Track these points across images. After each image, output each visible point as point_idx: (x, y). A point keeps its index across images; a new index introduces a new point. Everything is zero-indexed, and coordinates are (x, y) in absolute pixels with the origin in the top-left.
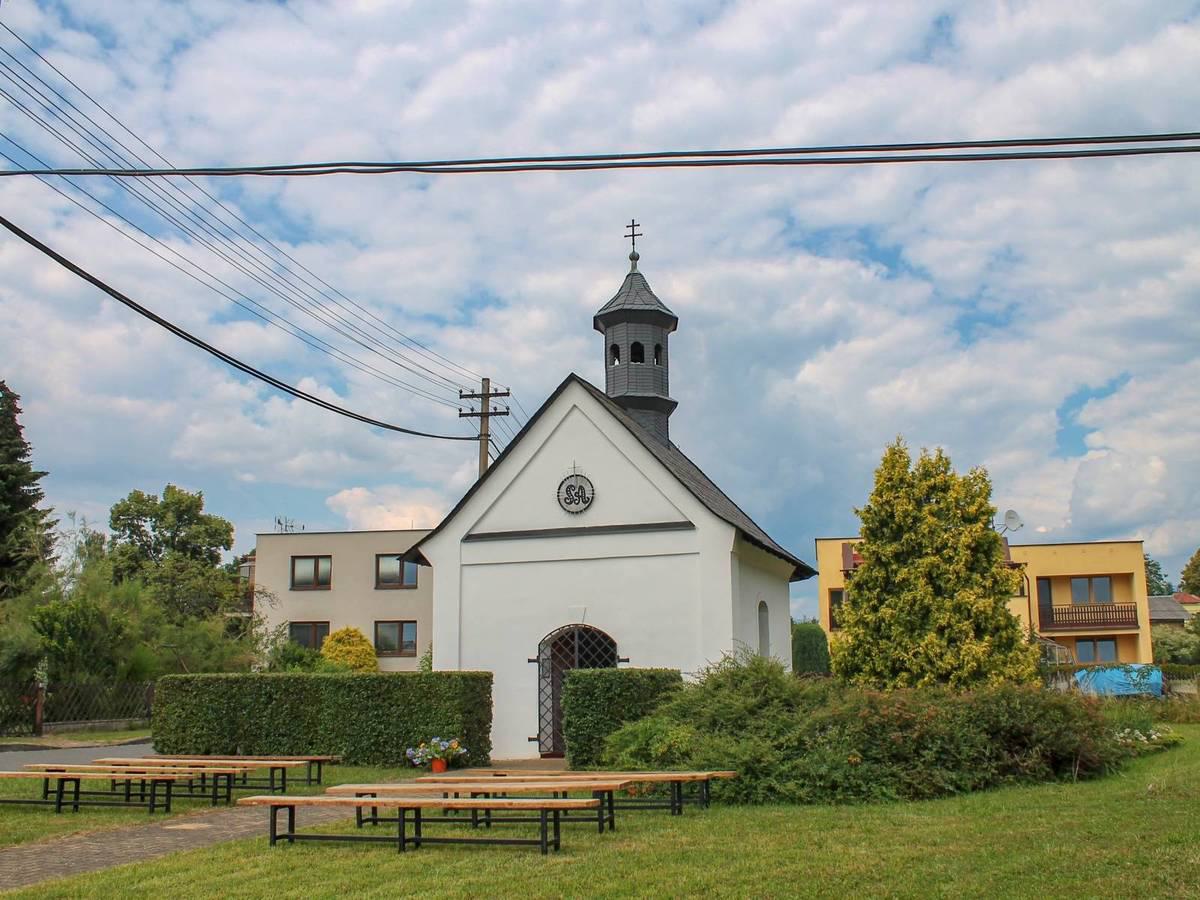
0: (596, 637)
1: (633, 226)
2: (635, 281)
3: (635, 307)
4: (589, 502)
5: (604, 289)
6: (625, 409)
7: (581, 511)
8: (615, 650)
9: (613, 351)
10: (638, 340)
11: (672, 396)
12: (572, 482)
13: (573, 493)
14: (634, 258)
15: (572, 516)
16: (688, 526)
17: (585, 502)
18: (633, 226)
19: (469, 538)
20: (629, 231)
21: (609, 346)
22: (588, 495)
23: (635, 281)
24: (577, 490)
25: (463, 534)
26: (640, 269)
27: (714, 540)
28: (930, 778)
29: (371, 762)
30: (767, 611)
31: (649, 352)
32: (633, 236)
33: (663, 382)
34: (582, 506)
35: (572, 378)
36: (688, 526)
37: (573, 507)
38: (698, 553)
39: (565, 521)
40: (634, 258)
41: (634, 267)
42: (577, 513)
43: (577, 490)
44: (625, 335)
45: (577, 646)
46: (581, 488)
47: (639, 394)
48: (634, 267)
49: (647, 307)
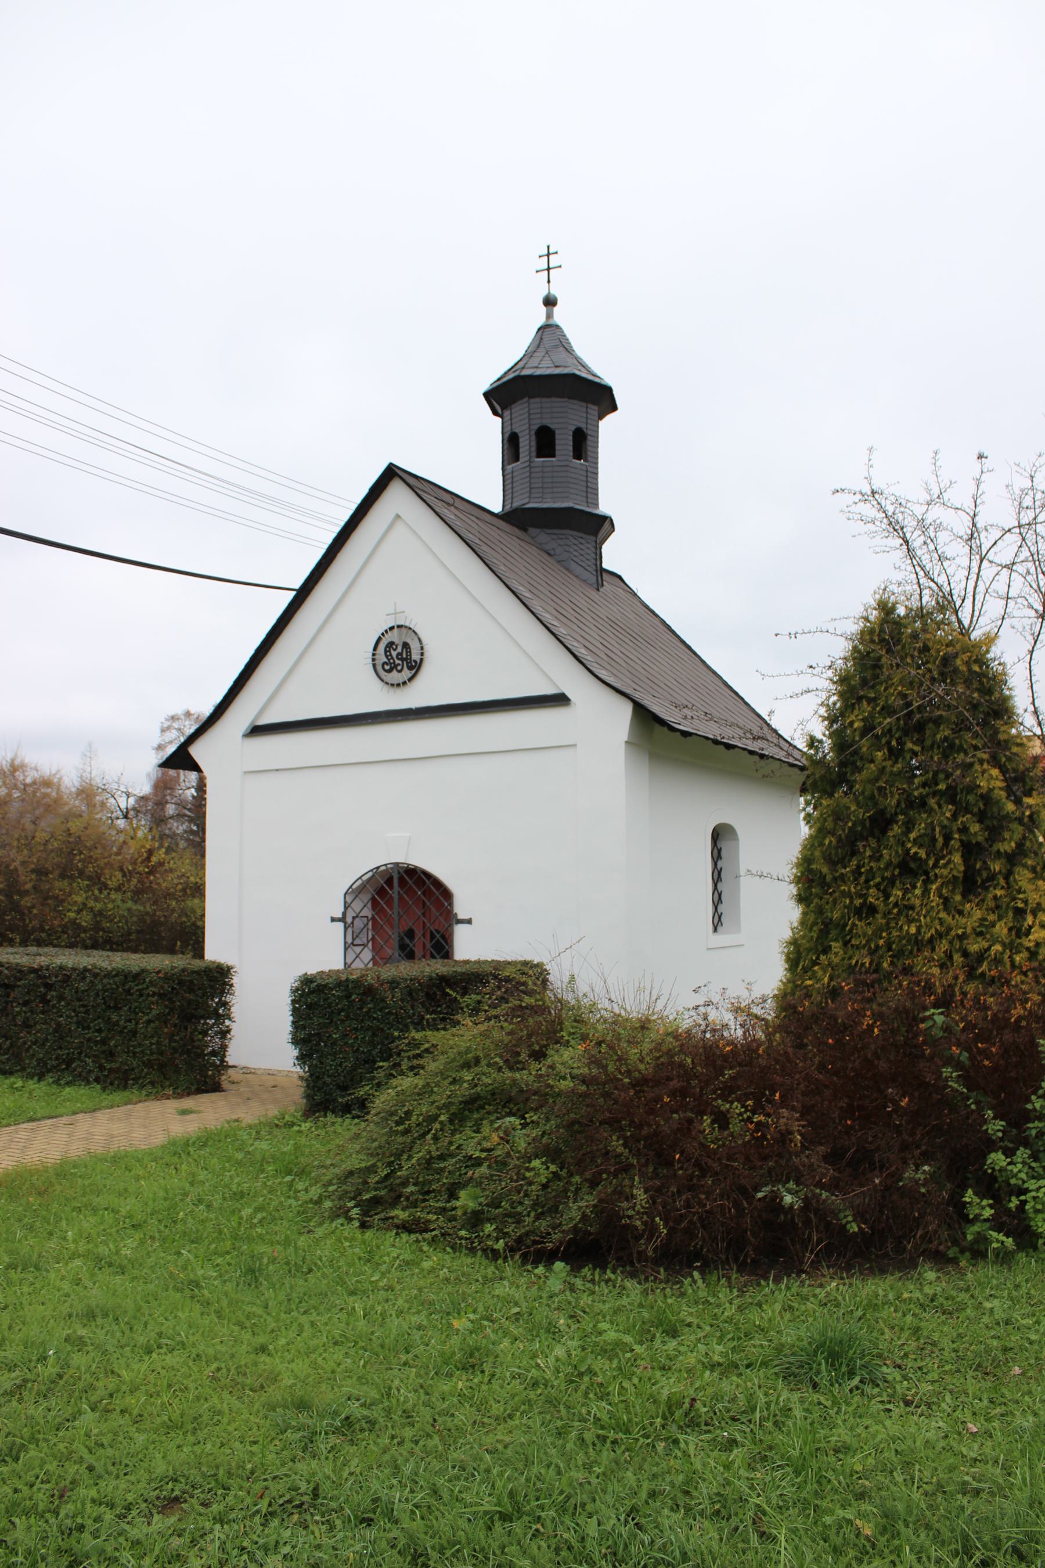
0: (424, 883)
1: (548, 255)
2: (549, 335)
3: (538, 372)
4: (416, 667)
5: (504, 353)
6: (525, 530)
7: (404, 683)
8: (451, 904)
9: (511, 444)
10: (547, 422)
11: (605, 507)
12: (394, 637)
13: (394, 654)
14: (550, 302)
15: (392, 690)
16: (560, 700)
17: (410, 668)
18: (548, 255)
19: (256, 731)
20: (554, 261)
21: (507, 436)
22: (416, 656)
23: (549, 335)
24: (399, 649)
25: (245, 725)
26: (560, 315)
27: (600, 723)
28: (261, 1339)
29: (83, 1078)
30: (737, 839)
31: (564, 443)
32: (549, 269)
33: (591, 490)
34: (407, 674)
35: (391, 474)
36: (560, 700)
37: (395, 677)
38: (575, 745)
39: (379, 698)
40: (550, 302)
41: (549, 316)
42: (398, 685)
43: (399, 649)
44: (529, 414)
45: (396, 896)
46: (406, 645)
47: (545, 506)
48: (549, 316)
49: (557, 371)
